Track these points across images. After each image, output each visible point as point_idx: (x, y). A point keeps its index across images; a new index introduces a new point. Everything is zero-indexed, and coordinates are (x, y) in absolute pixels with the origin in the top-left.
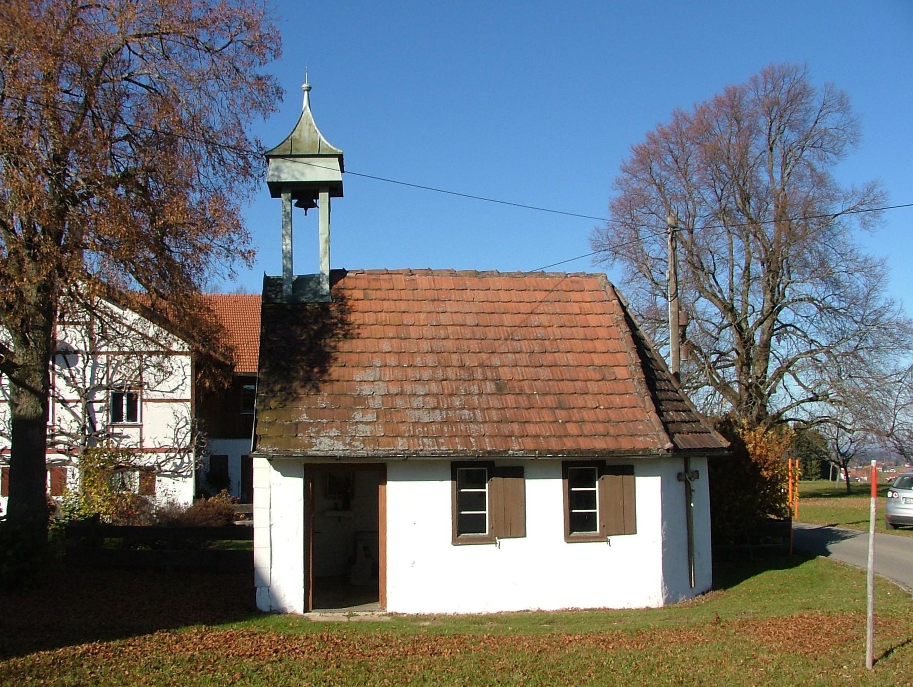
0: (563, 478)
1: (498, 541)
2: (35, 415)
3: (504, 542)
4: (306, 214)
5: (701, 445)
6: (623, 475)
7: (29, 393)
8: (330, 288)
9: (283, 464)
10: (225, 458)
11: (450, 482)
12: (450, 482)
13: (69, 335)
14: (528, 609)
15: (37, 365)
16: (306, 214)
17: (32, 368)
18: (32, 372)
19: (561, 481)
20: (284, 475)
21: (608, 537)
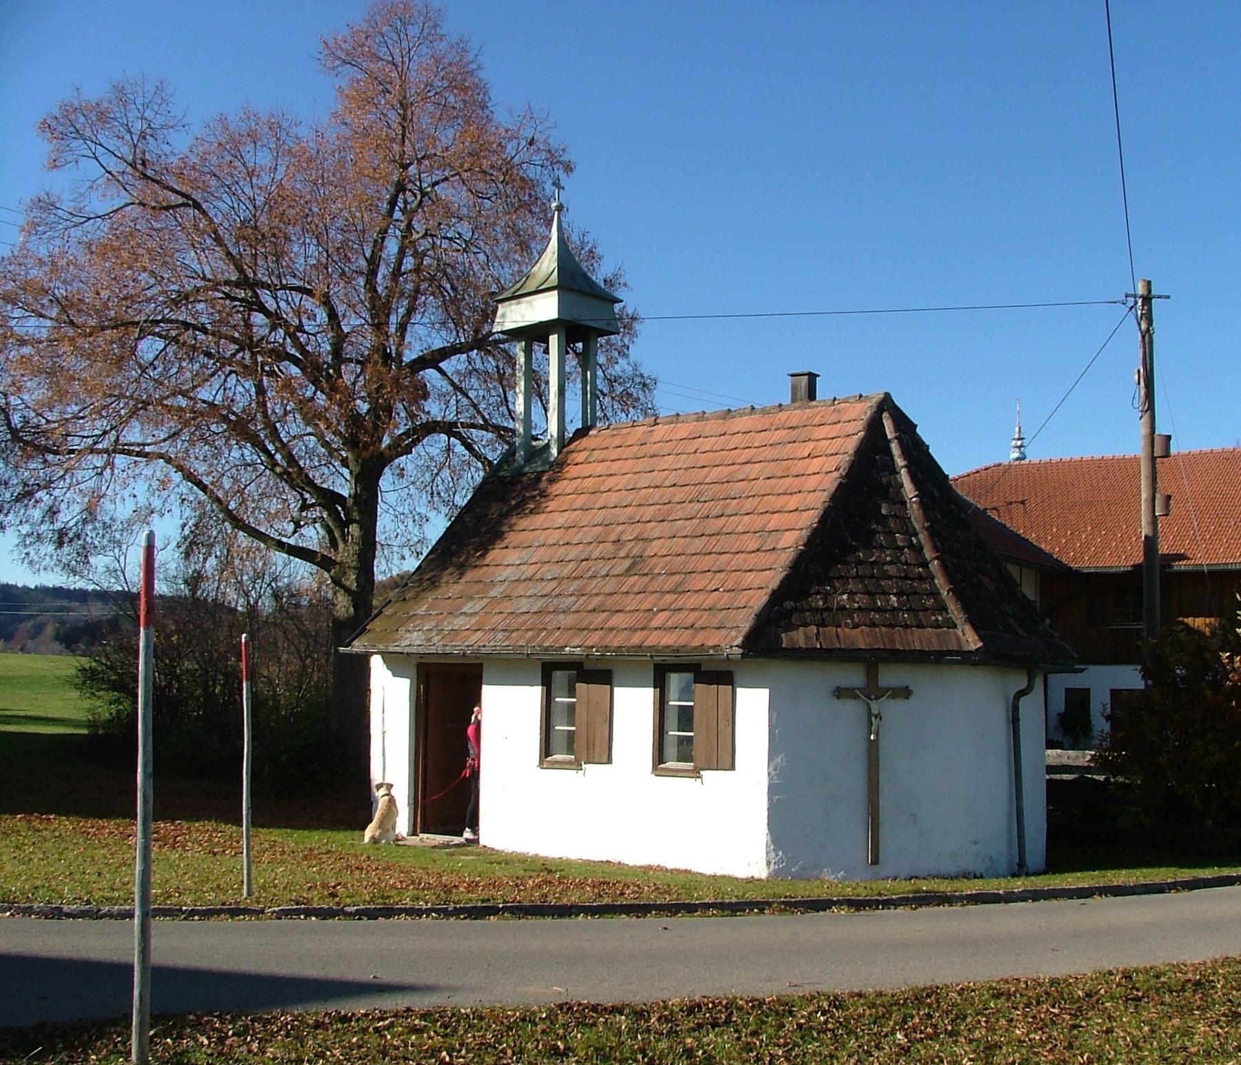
0: (655, 687)
1: (584, 766)
2: (346, 616)
3: (589, 768)
4: (1168, 297)
5: (941, 645)
6: (718, 684)
7: (343, 592)
8: (559, 453)
9: (396, 663)
10: (1087, 691)
11: (619, 692)
12: (619, 692)
13: (996, 505)
14: (609, 860)
15: (352, 561)
16: (1168, 297)
17: (347, 565)
18: (347, 570)
19: (652, 690)
20: (394, 676)
21: (701, 772)
